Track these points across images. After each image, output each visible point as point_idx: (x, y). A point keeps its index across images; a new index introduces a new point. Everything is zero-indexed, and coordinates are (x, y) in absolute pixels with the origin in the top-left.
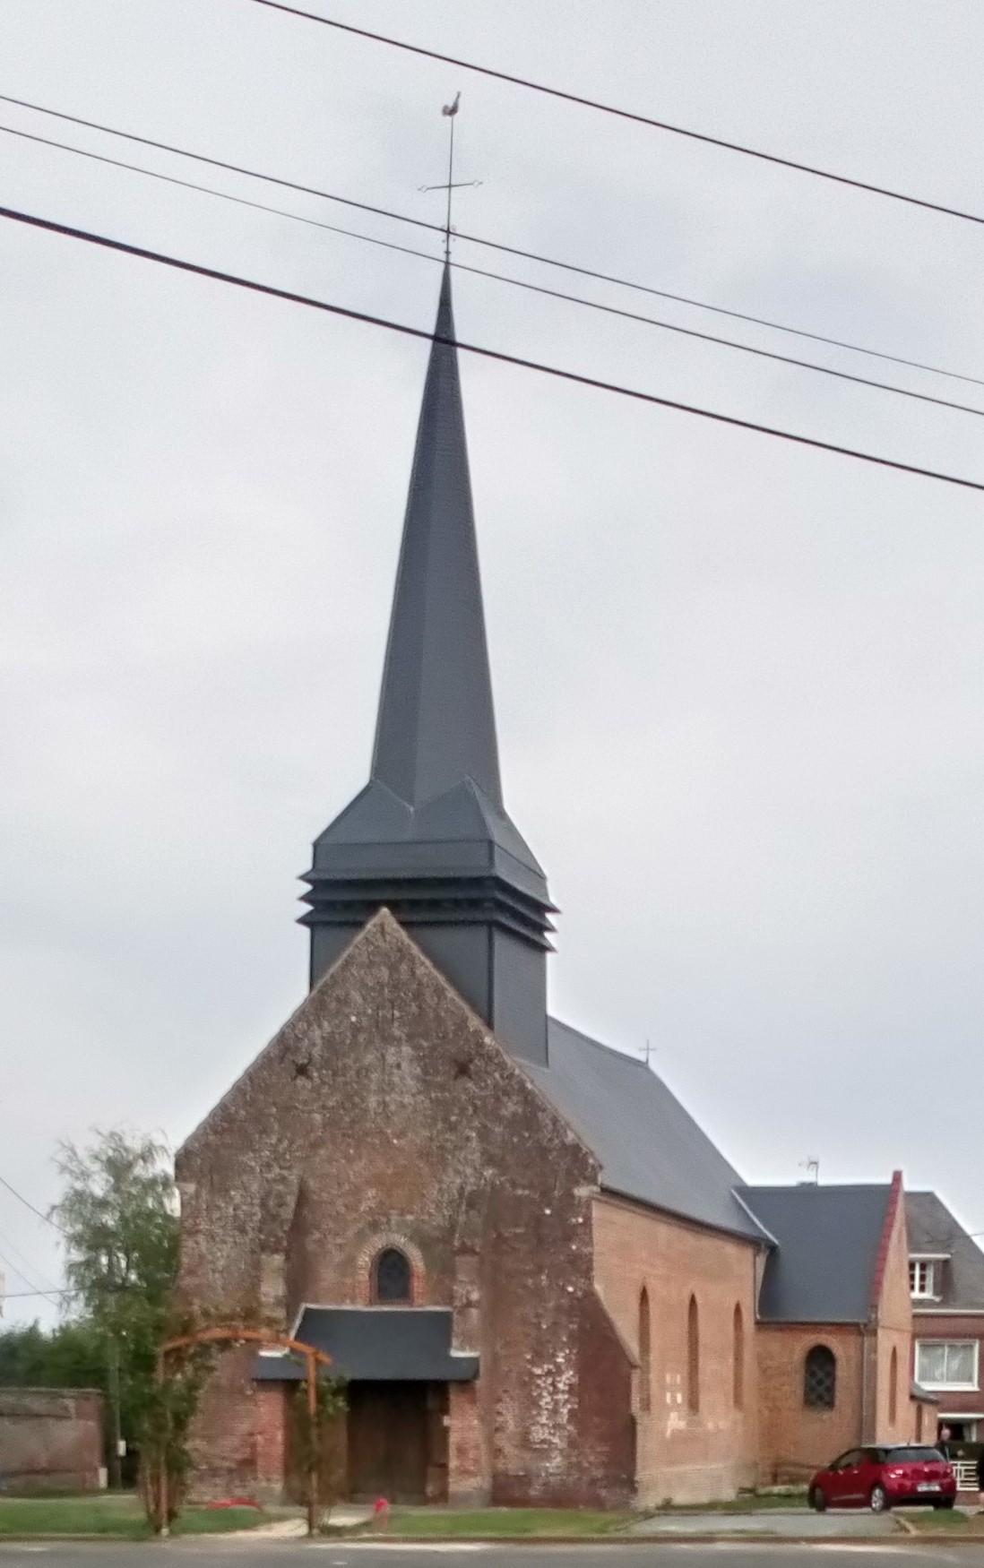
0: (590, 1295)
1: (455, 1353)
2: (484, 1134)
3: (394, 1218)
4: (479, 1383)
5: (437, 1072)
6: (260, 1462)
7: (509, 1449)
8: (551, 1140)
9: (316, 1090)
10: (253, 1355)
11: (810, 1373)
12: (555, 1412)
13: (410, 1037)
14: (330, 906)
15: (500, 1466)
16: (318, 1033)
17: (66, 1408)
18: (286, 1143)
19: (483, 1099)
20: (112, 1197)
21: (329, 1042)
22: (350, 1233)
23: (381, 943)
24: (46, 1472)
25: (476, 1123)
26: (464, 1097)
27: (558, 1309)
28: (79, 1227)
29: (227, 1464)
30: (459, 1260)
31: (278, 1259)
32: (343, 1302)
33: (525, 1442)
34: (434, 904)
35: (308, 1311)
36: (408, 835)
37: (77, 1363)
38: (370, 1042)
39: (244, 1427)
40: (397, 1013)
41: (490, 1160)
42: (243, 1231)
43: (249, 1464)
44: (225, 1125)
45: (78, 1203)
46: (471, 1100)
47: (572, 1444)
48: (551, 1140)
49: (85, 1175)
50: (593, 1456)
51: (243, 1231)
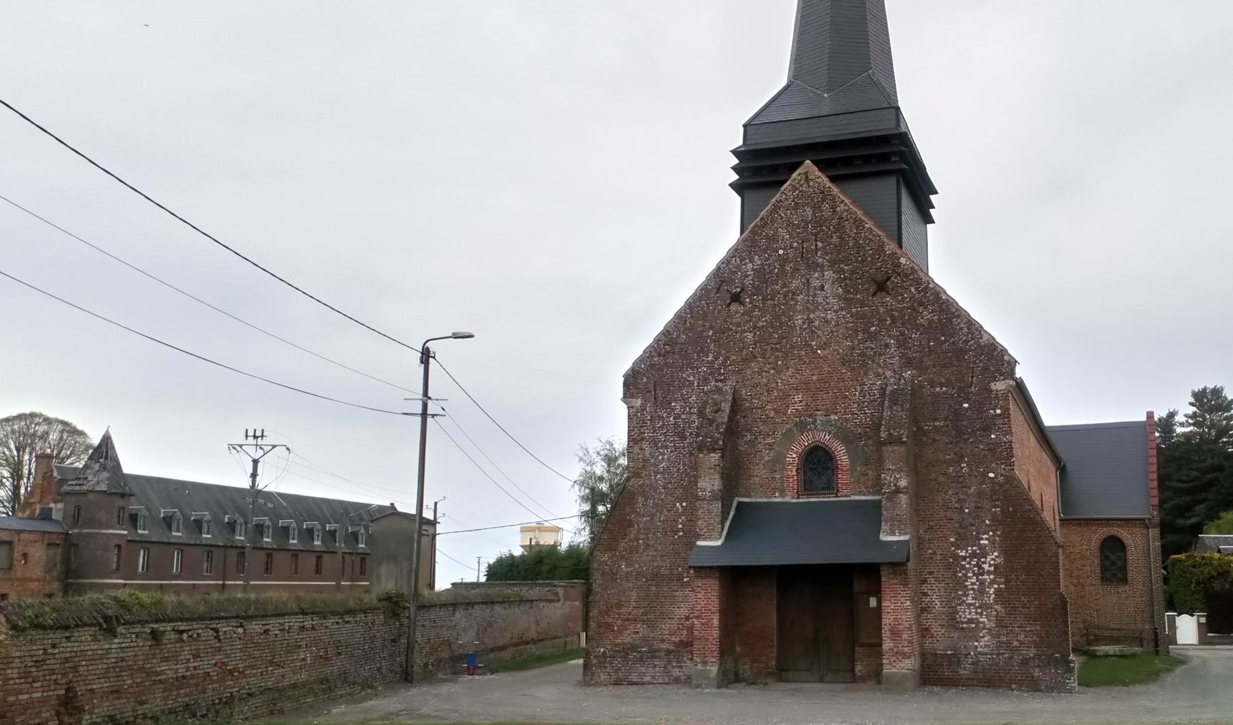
0: (1011, 480)
1: (885, 538)
2: (902, 343)
4: (910, 565)
5: (857, 292)
7: (936, 629)
8: (966, 342)
9: (748, 313)
10: (691, 545)
12: (981, 592)
13: (832, 264)
14: (757, 171)
17: (557, 594)
20: (606, 475)
21: (760, 273)
22: (779, 434)
24: (534, 642)
25: (895, 332)
26: (881, 310)
27: (980, 494)
31: (715, 457)
32: (773, 495)
33: (952, 622)
34: (847, 162)
35: (740, 504)
38: (796, 270)
39: (683, 611)
40: (820, 245)
41: (908, 363)
42: (683, 438)
43: (686, 646)
46: (889, 312)
47: (1000, 623)
48: (966, 342)
49: (591, 464)
50: (1024, 637)
51: (683, 438)
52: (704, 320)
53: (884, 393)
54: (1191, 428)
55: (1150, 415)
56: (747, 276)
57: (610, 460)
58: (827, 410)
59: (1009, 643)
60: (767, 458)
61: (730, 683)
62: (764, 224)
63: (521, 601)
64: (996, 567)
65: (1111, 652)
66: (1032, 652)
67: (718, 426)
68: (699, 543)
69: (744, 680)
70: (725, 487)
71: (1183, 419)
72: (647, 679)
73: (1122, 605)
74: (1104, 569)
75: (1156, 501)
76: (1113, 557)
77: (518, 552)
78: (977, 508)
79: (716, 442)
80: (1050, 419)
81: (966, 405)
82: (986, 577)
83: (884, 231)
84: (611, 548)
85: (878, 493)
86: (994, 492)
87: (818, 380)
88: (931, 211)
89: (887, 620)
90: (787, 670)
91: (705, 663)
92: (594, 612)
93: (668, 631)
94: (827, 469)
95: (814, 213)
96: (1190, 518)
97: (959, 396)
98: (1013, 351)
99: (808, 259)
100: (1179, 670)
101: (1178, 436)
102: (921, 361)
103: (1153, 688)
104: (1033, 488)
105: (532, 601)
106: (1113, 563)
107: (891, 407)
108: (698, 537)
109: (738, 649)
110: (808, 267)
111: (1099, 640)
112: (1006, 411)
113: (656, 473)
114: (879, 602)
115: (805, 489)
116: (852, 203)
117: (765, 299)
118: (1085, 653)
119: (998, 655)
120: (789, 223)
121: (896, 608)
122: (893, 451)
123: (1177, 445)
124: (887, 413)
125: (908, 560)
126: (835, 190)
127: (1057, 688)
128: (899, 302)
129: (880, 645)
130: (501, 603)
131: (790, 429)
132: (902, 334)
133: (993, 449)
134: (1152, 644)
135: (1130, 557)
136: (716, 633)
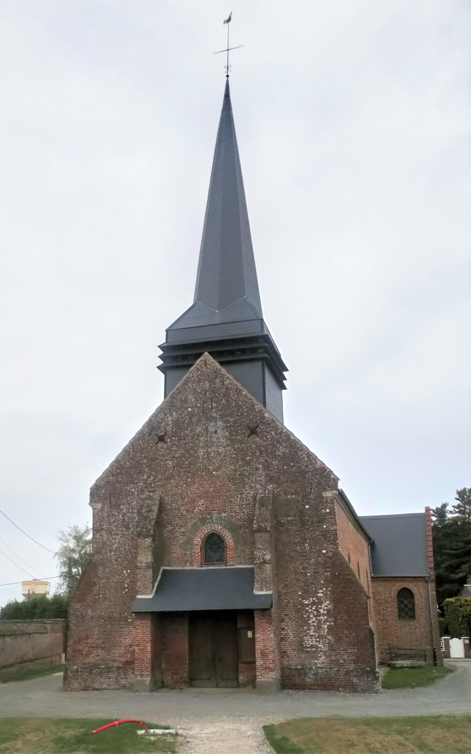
0: (337, 554)
2: (267, 467)
3: (215, 516)
5: (237, 434)
6: (137, 663)
7: (290, 652)
8: (307, 466)
10: (133, 598)
11: (400, 602)
12: (319, 627)
14: (175, 358)
15: (285, 663)
16: (170, 418)
18: (152, 478)
19: (265, 446)
21: (176, 423)
23: (204, 369)
26: (253, 446)
27: (317, 563)
28: (65, 559)
29: (116, 664)
30: (258, 535)
31: (148, 541)
33: (301, 647)
34: (231, 353)
35: (164, 571)
36: (217, 322)
37: (59, 608)
38: (199, 421)
39: (128, 641)
40: (214, 405)
41: (270, 479)
42: (128, 528)
43: (130, 664)
44: (118, 471)
45: (66, 552)
47: (331, 648)
48: (307, 466)
50: (347, 656)
51: (128, 528)
52: (141, 453)
53: (255, 499)
54: (457, 515)
55: (427, 509)
56: (168, 425)
57: (78, 538)
58: (219, 510)
59: (337, 660)
60: (181, 541)
61: (159, 688)
62: (179, 392)
63: (23, 634)
64: (328, 611)
65: (405, 665)
66: (352, 667)
67: (150, 521)
68: (139, 597)
69: (167, 687)
70: (155, 559)
71: (452, 509)
72: (104, 686)
73: (413, 633)
74: (400, 610)
75: (432, 565)
76: (406, 602)
77: (21, 599)
78: (315, 572)
79: (149, 531)
80: (360, 512)
81: (307, 507)
82: (322, 617)
83: (254, 396)
84: (81, 600)
85: (253, 564)
86: (326, 563)
87: (214, 491)
88: (284, 382)
89: (259, 646)
90: (195, 680)
91: (142, 675)
92: (70, 643)
93: (118, 654)
94: (220, 548)
95: (210, 386)
96: (459, 573)
97: (303, 501)
98: (336, 472)
99: (207, 414)
100: (449, 676)
101: (449, 519)
102: (279, 479)
103: (430, 689)
104: (352, 558)
105: (30, 634)
106: (406, 606)
107: (260, 508)
108: (138, 593)
109: (164, 666)
110: (207, 419)
111: (398, 657)
112: (332, 510)
113: (111, 551)
114: (254, 634)
115: (206, 561)
116: (235, 378)
117: (179, 439)
118: (389, 665)
119: (331, 668)
120: (195, 391)
121: (264, 638)
122: (261, 537)
123: (450, 525)
124: (257, 512)
125: (271, 607)
126: (223, 371)
127: (368, 690)
128: (264, 441)
129: (254, 662)
130: (10, 635)
131: (196, 522)
132: (266, 461)
133: (325, 534)
134: (432, 658)
135: (416, 602)
136: (149, 656)
